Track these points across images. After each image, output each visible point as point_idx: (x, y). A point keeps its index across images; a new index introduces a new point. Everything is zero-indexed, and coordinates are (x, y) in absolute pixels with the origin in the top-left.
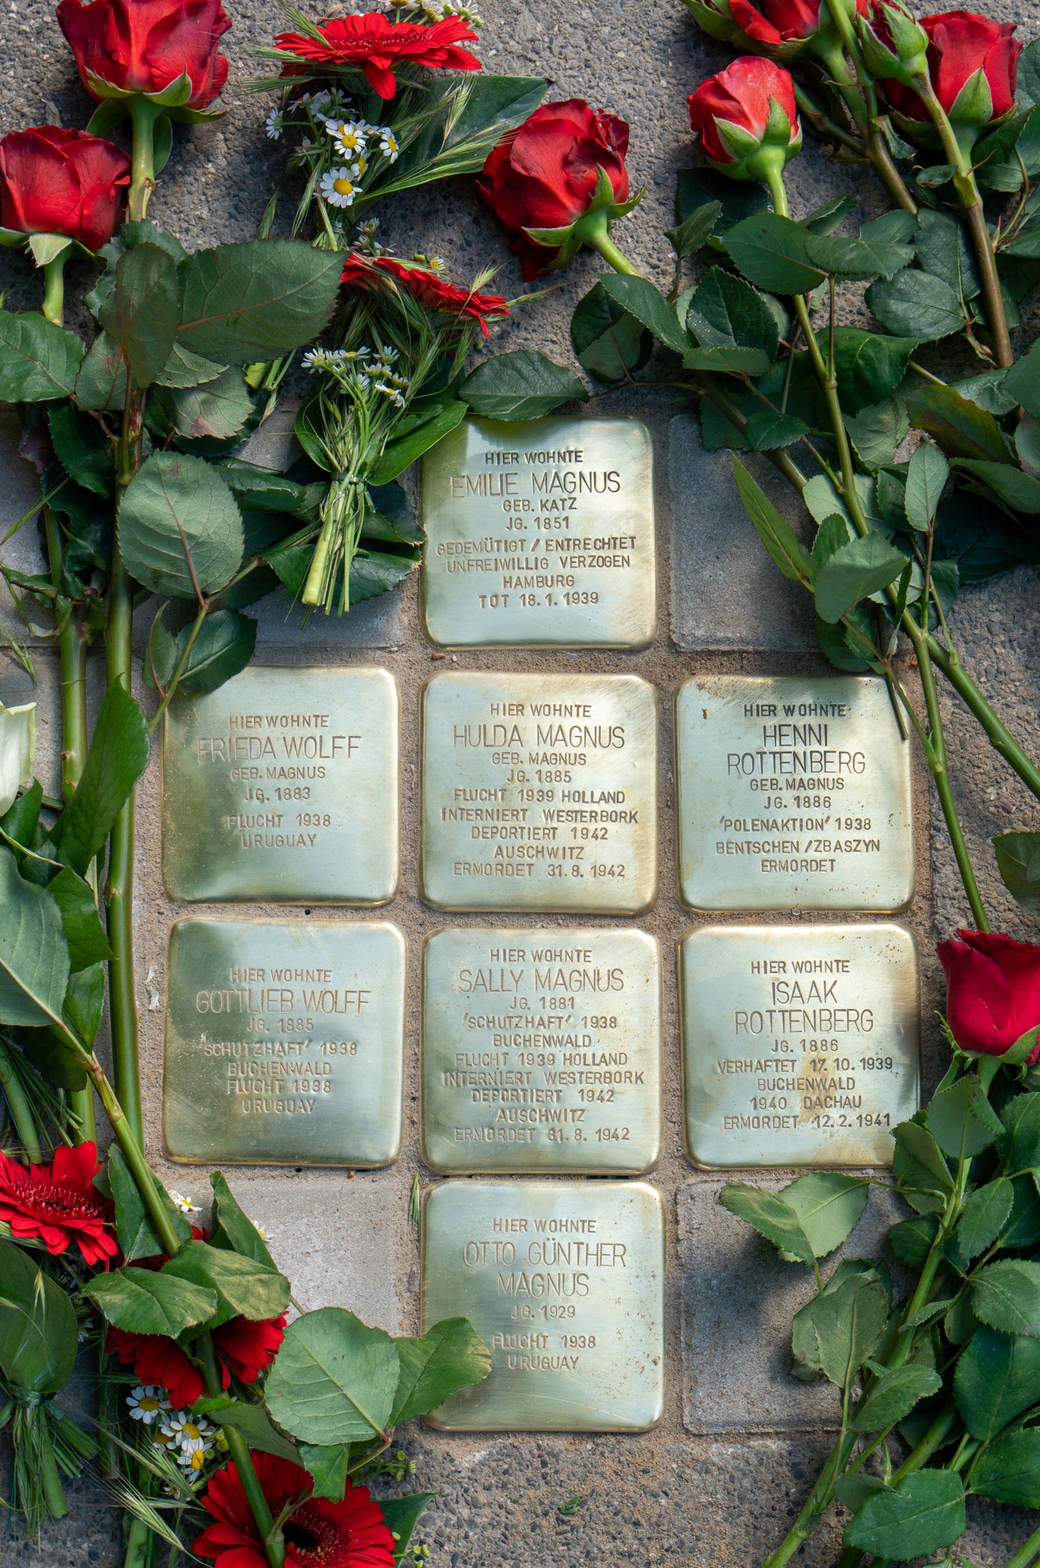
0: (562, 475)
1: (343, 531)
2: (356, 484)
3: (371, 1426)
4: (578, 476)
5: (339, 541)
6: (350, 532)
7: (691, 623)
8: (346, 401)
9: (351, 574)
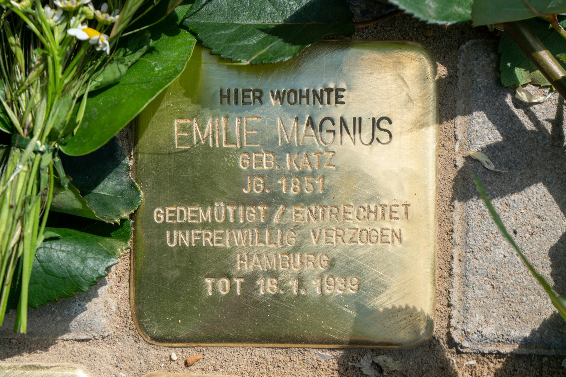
0: (317, 121)
1: (22, 219)
2: (42, 153)
3: (119, 69)
4: (338, 122)
5: (18, 233)
6: (34, 211)
7: (478, 318)
8: (31, 40)
9: (34, 269)
